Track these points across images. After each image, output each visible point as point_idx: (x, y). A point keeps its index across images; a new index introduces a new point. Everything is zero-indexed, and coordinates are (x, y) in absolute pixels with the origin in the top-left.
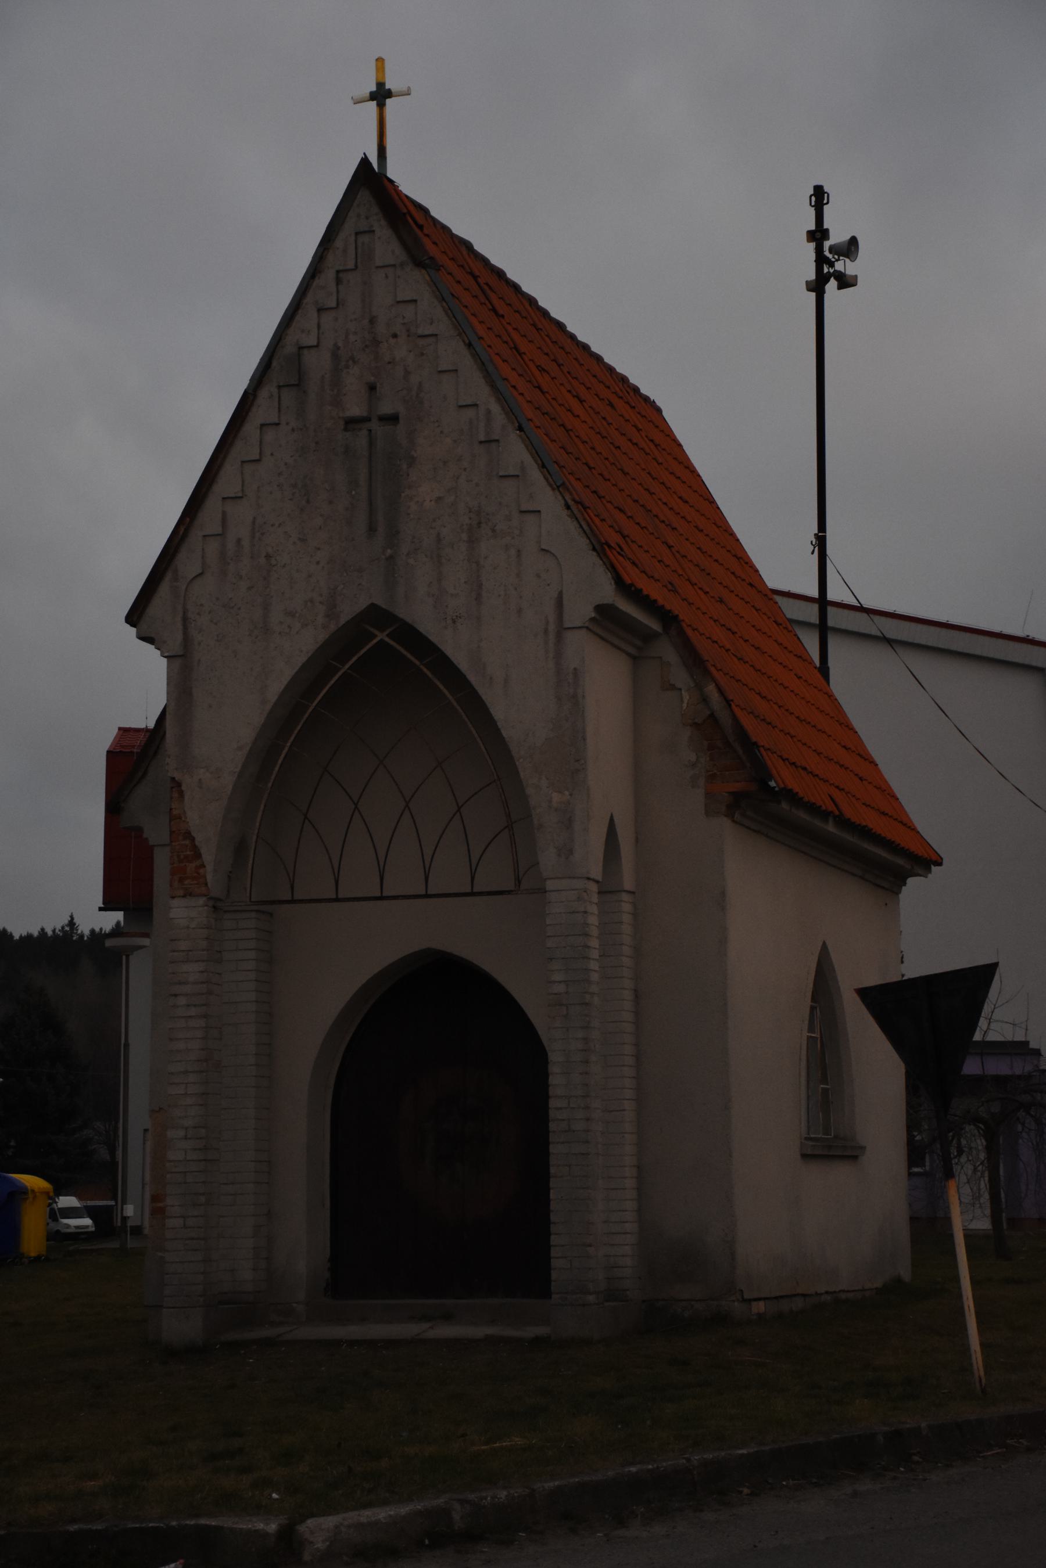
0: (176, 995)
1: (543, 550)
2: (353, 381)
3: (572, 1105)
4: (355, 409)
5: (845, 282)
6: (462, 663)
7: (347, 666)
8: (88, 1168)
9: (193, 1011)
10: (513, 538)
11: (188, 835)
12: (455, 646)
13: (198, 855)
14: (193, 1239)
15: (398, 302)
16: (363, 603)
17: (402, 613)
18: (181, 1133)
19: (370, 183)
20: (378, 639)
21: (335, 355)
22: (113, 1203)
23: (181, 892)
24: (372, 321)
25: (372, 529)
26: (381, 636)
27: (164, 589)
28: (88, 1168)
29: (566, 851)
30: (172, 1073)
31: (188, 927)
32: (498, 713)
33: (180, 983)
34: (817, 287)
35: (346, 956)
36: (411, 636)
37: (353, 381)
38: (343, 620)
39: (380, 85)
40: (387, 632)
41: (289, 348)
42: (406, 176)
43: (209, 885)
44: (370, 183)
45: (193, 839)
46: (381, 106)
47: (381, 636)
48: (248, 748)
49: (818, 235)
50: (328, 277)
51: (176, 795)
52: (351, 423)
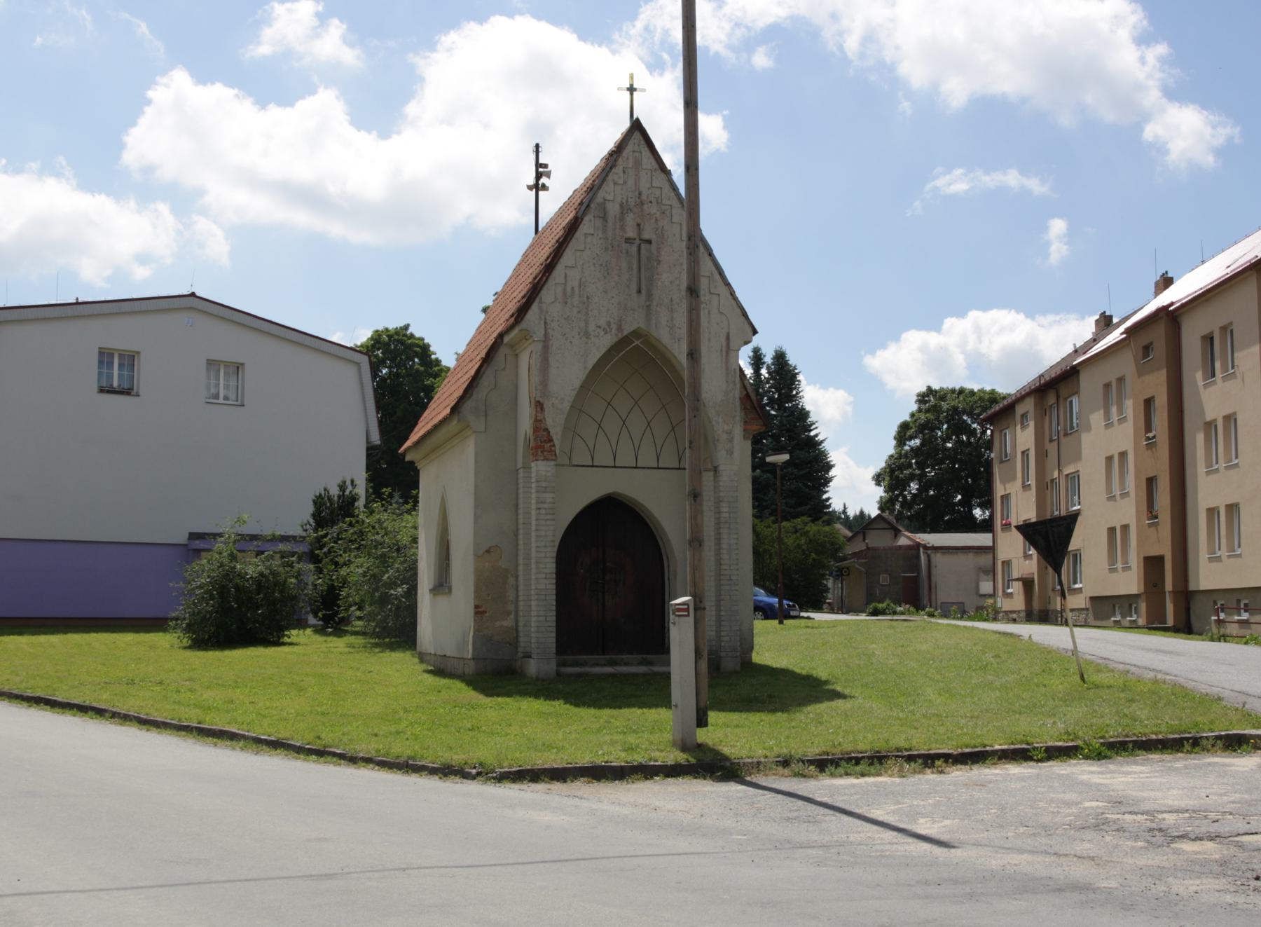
2: (630, 220)
4: (631, 233)
8: (988, 504)
9: (549, 517)
11: (546, 430)
13: (551, 440)
16: (633, 328)
19: (636, 127)
21: (621, 205)
22: (443, 620)
24: (640, 194)
25: (639, 292)
26: (637, 343)
28: (988, 504)
29: (730, 452)
37: (630, 220)
38: (625, 333)
39: (632, 85)
46: (632, 94)
47: (637, 343)
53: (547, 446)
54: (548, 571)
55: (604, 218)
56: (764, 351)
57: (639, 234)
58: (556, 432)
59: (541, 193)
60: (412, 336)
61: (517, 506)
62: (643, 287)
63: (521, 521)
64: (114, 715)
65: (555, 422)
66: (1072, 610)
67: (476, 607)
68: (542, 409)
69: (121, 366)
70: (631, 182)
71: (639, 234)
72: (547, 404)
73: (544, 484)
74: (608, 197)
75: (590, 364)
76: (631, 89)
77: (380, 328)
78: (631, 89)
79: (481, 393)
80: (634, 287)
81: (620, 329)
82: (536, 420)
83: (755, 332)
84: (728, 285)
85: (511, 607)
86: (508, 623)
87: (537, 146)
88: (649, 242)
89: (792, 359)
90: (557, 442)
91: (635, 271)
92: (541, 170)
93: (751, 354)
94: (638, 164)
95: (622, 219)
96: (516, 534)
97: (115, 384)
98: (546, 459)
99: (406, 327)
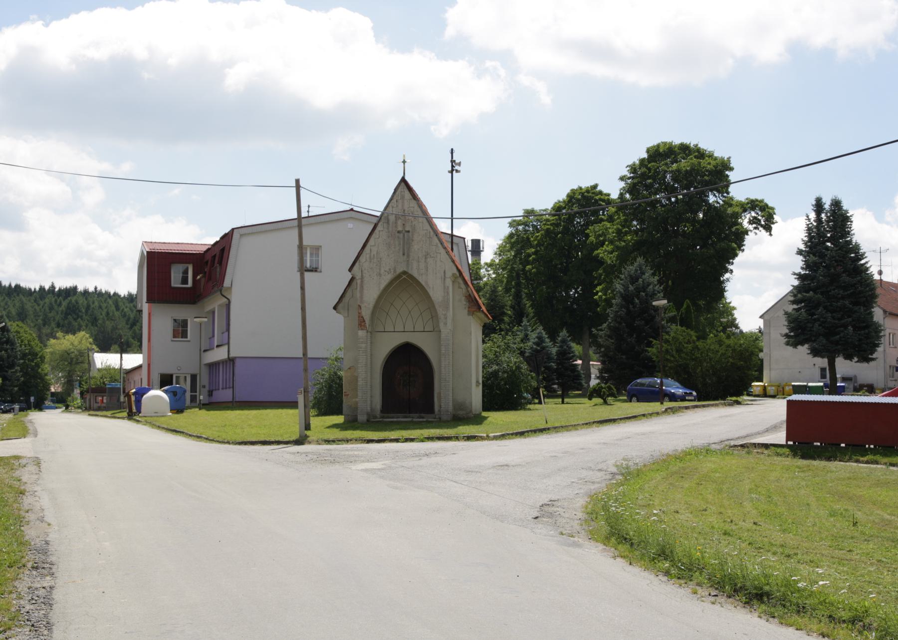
2: (400, 222)
4: (400, 229)
5: (457, 171)
6: (423, 283)
12: (422, 280)
13: (364, 321)
17: (410, 272)
19: (403, 181)
27: (357, 264)
29: (446, 324)
32: (431, 294)
34: (452, 172)
35: (388, 343)
36: (411, 277)
37: (400, 222)
41: (386, 215)
42: (406, 178)
44: (403, 181)
49: (453, 161)
50: (394, 201)
52: (399, 232)
55: (388, 223)
56: (824, 201)
58: (367, 318)
60: (601, 193)
64: (187, 434)
66: (293, 405)
69: (311, 254)
70: (400, 206)
72: (363, 306)
75: (382, 286)
76: (404, 162)
77: (575, 187)
79: (346, 300)
80: (401, 253)
81: (395, 271)
88: (408, 232)
89: (845, 206)
93: (814, 203)
94: (403, 197)
95: (396, 223)
97: (308, 266)
99: (595, 186)
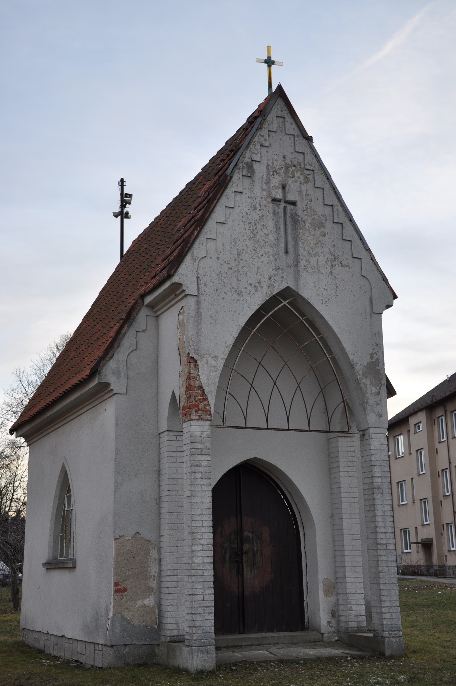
0: (195, 472)
1: (363, 276)
3: (387, 537)
7: (269, 315)
9: (205, 482)
10: (350, 268)
13: (206, 399)
14: (208, 607)
15: (296, 152)
18: (200, 548)
19: (278, 96)
20: (283, 304)
23: (197, 417)
25: (287, 251)
26: (285, 303)
30: (194, 515)
31: (201, 436)
33: (197, 466)
38: (274, 294)
39: (269, 58)
40: (287, 301)
43: (212, 415)
45: (203, 391)
46: (269, 66)
47: (285, 303)
48: (230, 347)
51: (192, 366)
53: (201, 405)
54: (204, 542)
57: (284, 195)
59: (125, 220)
61: (159, 473)
62: (290, 248)
63: (164, 488)
65: (209, 377)
67: (116, 584)
68: (196, 366)
71: (284, 195)
73: (199, 446)
74: (255, 158)
76: (269, 62)
78: (269, 62)
81: (271, 286)
82: (189, 378)
83: (395, 297)
84: (369, 250)
85: (153, 584)
86: (150, 601)
87: (122, 181)
88: (294, 203)
90: (212, 400)
91: (282, 232)
92: (125, 199)
96: (159, 500)
98: (200, 419)
